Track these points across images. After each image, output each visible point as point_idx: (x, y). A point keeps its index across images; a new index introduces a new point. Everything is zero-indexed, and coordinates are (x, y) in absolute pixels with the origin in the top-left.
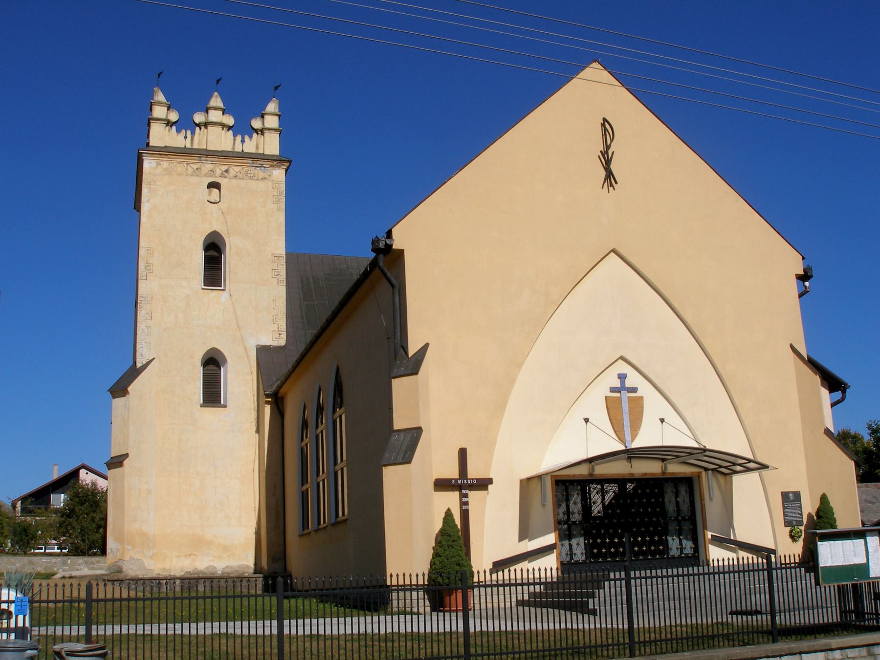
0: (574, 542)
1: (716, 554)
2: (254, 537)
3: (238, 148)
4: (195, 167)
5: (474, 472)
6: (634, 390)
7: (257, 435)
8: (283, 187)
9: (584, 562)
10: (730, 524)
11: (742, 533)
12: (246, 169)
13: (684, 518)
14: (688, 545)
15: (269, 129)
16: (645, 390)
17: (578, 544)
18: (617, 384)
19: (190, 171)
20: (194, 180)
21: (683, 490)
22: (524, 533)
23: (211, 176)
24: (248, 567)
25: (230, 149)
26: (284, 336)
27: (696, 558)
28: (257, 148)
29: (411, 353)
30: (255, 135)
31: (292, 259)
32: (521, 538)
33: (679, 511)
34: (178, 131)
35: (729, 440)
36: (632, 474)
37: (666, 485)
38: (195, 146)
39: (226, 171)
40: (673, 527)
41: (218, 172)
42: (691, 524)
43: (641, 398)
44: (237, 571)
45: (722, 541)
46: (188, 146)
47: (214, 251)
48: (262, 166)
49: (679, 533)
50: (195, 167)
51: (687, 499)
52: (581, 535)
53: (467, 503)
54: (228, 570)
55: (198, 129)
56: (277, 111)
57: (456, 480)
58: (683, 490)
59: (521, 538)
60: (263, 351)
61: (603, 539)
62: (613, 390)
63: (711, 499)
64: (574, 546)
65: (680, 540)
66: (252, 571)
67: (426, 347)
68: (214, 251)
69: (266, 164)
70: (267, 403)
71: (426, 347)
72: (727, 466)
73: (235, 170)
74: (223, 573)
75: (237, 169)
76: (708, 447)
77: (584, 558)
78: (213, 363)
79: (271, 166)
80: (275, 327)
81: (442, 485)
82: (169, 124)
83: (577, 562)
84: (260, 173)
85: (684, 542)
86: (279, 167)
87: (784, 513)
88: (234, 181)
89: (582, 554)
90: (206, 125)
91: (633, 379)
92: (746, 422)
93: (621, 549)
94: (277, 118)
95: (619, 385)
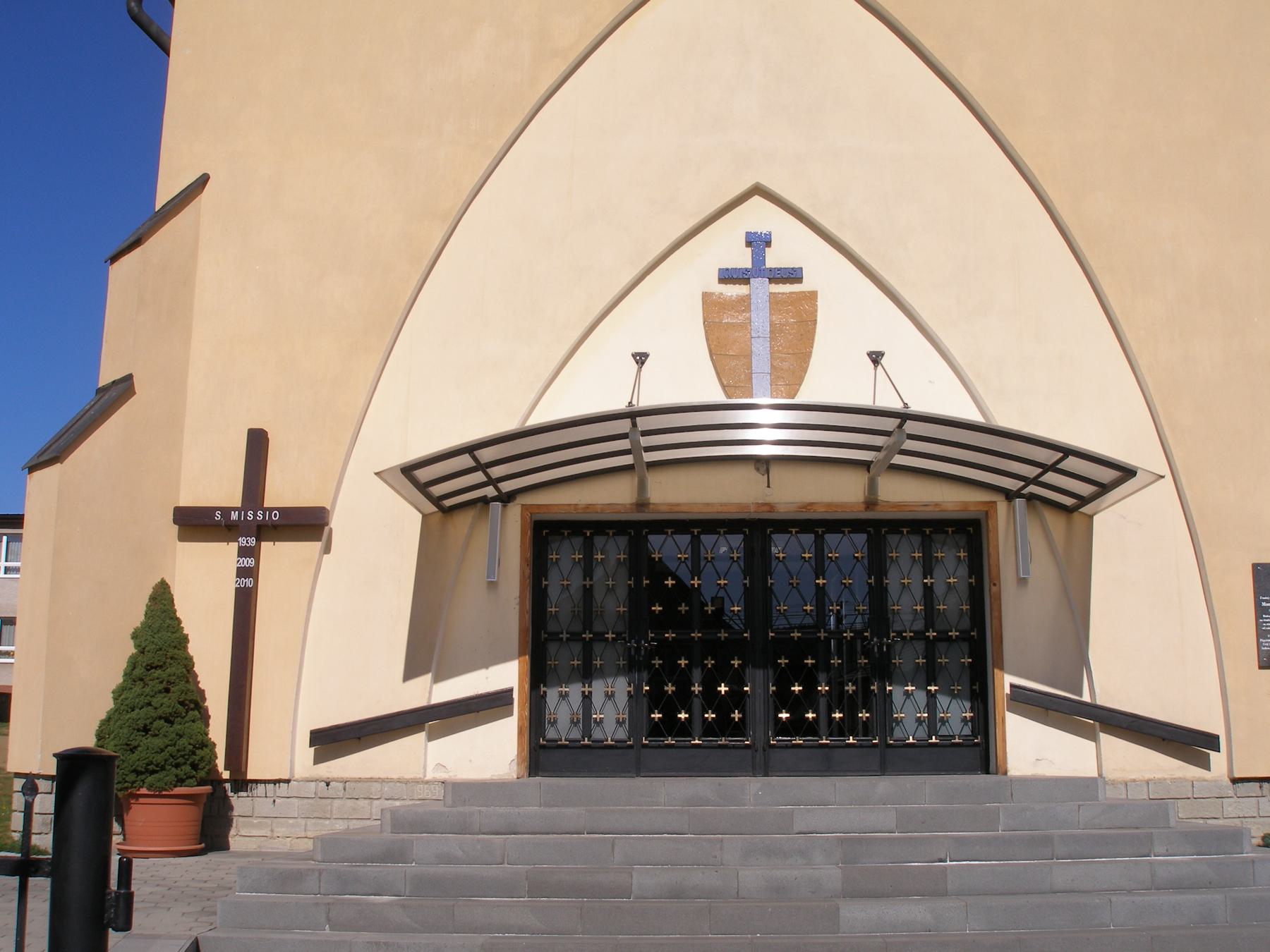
0: (598, 688)
1: (1030, 747)
5: (282, 490)
6: (793, 276)
9: (619, 746)
10: (1081, 660)
11: (1108, 685)
13: (944, 637)
14: (955, 713)
16: (824, 272)
17: (610, 696)
18: (744, 259)
21: (424, 474)
22: (420, 659)
27: (980, 751)
32: (412, 670)
33: (930, 615)
35: (1088, 411)
36: (771, 507)
37: (893, 539)
40: (909, 658)
42: (966, 653)
43: (812, 296)
45: (1033, 705)
49: (929, 674)
51: (893, 581)
52: (619, 672)
53: (242, 572)
57: (226, 511)
58: (950, 557)
59: (412, 670)
61: (810, 685)
62: (727, 277)
63: (1022, 582)
64: (598, 699)
65: (931, 696)
72: (1066, 487)
76: (916, 407)
77: (967, 731)
81: (197, 523)
83: (599, 746)
85: (943, 700)
87: (1258, 626)
89: (620, 723)
91: (792, 245)
92: (1142, 362)
93: (736, 715)
95: (748, 264)
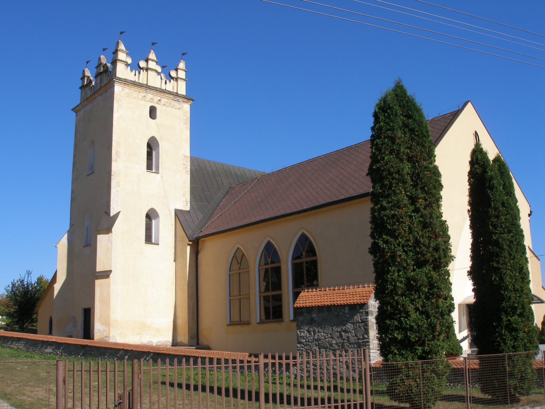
2: (172, 324)
3: (163, 87)
4: (143, 95)
7: (174, 263)
8: (189, 115)
12: (170, 101)
15: (181, 79)
19: (140, 97)
20: (142, 103)
23: (151, 102)
24: (169, 341)
25: (159, 87)
26: (189, 204)
28: (173, 89)
29: (112, 215)
30: (172, 80)
31: (193, 160)
34: (132, 70)
38: (141, 82)
39: (160, 100)
41: (155, 101)
44: (163, 344)
46: (137, 81)
47: (152, 147)
48: (178, 101)
50: (143, 95)
54: (159, 344)
55: (142, 71)
56: (184, 68)
60: (178, 214)
66: (170, 344)
67: (118, 214)
68: (152, 147)
69: (181, 100)
70: (189, 245)
71: (118, 214)
73: (164, 100)
74: (156, 345)
75: (166, 100)
78: (151, 216)
79: (183, 102)
80: (184, 199)
82: (127, 65)
84: (176, 104)
86: (187, 103)
88: (164, 107)
90: (147, 69)
94: (184, 73)
